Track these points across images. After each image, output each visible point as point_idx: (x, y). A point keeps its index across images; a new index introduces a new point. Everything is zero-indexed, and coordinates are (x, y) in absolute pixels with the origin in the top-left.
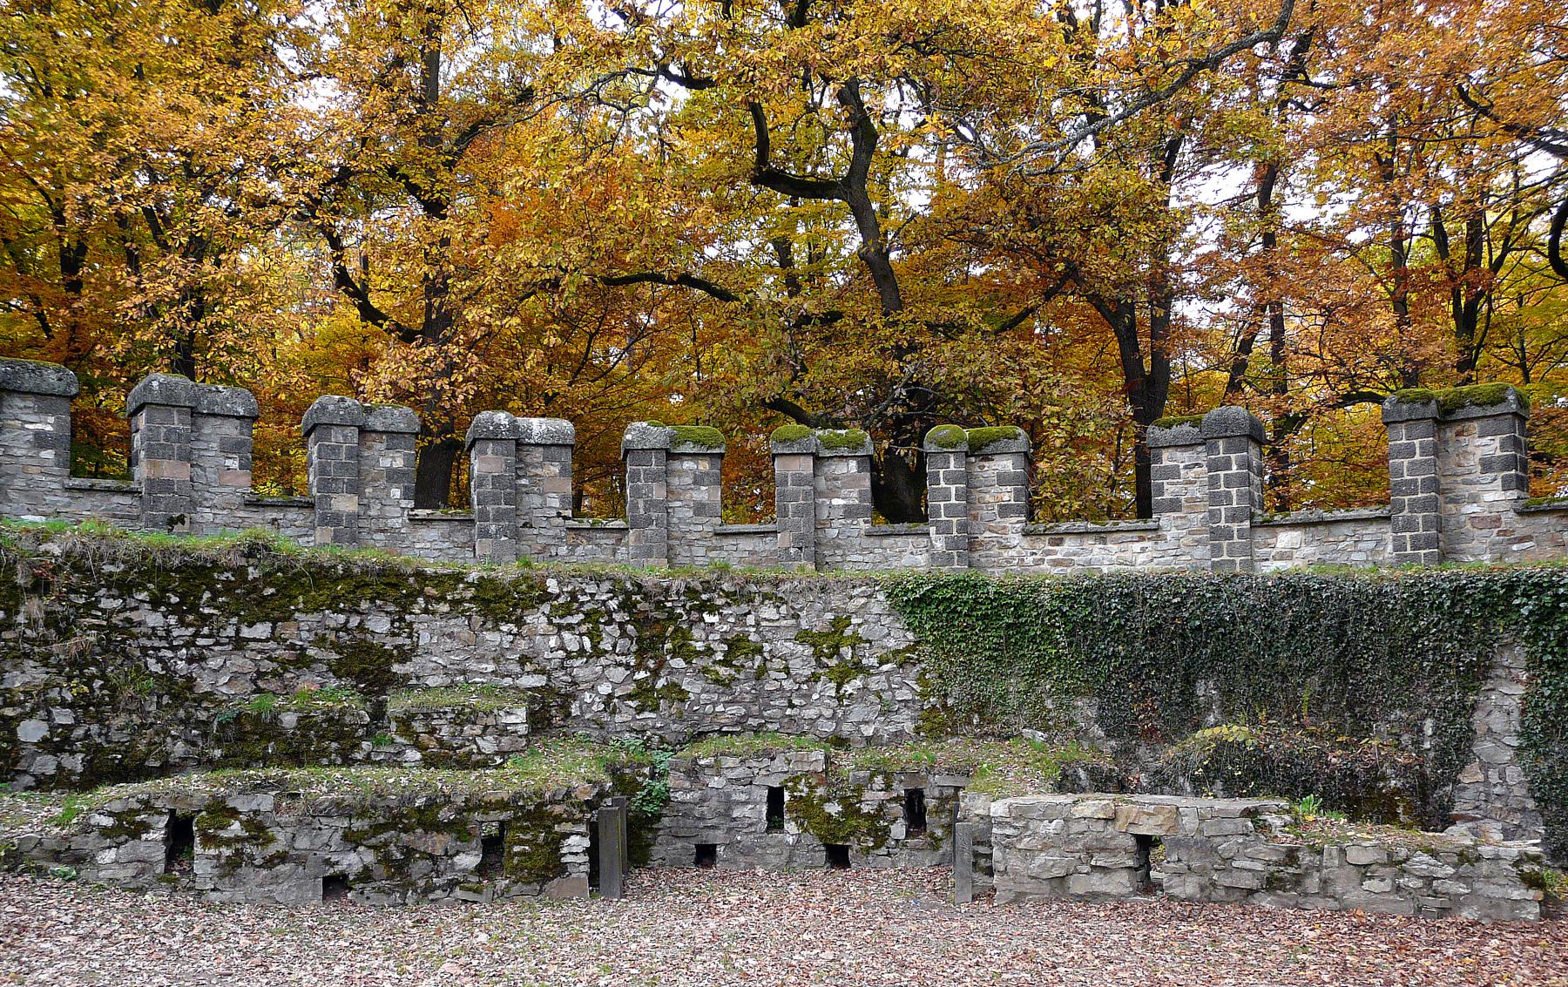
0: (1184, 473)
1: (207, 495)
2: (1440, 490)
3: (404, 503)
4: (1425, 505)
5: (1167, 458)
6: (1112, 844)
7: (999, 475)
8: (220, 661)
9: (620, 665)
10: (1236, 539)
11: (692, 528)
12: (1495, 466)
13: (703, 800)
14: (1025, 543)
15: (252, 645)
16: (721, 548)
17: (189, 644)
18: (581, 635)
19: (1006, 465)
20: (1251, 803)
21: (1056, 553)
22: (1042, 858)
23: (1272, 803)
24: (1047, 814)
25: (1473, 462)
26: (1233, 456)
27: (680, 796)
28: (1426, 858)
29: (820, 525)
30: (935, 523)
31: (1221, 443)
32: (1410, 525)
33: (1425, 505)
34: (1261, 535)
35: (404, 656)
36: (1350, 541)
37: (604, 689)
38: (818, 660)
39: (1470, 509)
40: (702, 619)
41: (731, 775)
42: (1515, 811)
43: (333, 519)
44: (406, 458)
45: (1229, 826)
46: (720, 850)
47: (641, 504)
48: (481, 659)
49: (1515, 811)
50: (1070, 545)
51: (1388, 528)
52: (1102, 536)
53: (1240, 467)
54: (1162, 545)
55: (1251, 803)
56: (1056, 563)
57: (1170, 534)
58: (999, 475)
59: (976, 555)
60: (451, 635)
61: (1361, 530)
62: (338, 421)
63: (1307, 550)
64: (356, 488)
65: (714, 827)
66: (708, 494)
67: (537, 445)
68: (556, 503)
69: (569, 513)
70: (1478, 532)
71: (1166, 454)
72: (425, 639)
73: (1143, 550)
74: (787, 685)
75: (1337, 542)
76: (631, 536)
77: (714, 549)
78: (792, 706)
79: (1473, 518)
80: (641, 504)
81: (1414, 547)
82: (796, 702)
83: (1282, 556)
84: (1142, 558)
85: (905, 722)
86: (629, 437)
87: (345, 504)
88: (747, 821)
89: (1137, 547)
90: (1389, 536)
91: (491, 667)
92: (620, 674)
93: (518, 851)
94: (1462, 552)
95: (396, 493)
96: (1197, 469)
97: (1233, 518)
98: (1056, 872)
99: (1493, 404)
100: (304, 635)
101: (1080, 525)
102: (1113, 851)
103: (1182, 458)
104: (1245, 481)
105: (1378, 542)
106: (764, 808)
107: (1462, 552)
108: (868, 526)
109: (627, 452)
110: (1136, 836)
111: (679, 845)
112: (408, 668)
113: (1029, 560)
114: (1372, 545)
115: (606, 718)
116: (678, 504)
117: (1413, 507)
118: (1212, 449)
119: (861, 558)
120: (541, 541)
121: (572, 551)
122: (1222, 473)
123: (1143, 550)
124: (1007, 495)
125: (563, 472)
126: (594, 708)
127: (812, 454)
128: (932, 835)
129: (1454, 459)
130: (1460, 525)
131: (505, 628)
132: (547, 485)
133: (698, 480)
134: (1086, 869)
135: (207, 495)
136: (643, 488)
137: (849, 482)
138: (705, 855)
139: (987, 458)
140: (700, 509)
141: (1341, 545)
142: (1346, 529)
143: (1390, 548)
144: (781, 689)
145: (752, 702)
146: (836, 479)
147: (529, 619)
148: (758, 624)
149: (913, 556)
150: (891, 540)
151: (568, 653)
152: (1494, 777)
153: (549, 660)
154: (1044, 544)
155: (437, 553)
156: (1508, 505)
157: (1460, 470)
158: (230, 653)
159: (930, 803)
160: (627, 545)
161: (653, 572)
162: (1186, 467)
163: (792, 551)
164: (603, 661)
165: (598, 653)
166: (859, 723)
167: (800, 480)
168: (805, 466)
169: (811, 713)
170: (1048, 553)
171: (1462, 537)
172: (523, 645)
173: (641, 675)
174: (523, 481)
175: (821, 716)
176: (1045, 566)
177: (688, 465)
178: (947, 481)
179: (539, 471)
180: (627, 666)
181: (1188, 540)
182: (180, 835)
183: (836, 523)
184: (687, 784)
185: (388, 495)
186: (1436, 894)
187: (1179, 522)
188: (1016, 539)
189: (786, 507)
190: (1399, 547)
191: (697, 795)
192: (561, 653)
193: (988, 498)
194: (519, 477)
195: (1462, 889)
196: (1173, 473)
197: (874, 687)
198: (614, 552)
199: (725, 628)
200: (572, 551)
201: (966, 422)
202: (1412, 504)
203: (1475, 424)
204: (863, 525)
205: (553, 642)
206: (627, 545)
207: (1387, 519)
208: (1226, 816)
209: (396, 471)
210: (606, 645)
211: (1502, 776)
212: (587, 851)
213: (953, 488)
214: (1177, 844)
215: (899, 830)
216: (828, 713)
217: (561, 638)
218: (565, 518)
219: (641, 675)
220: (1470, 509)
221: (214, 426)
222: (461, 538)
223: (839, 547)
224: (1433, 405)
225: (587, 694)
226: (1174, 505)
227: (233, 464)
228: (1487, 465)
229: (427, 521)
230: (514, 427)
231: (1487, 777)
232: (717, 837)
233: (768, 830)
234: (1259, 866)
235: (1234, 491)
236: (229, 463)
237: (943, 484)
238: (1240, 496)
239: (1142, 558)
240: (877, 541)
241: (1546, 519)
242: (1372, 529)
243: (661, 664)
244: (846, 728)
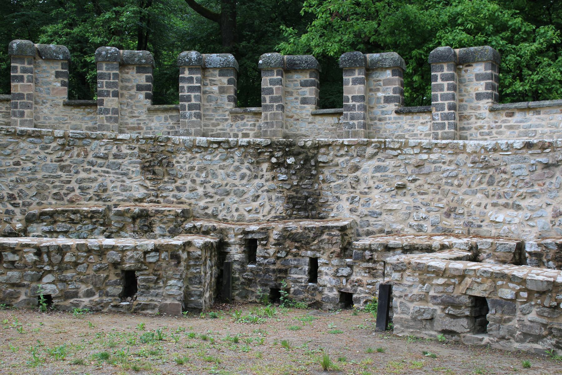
19: (479, 68)
60: (3, 364)
66: (310, 93)
110: (470, 296)
125: (229, 82)
137: (388, 84)
170: (504, 121)
178: (442, 80)
188: (485, 113)
229: (156, 110)
230: (199, 60)
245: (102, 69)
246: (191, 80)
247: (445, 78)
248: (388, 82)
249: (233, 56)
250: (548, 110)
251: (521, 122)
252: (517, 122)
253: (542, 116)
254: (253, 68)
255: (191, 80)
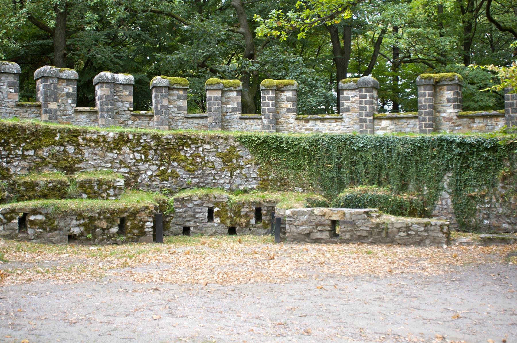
0: (351, 99)
1: (3, 102)
2: (435, 108)
3: (73, 105)
4: (429, 113)
5: (345, 94)
6: (324, 223)
7: (287, 98)
8: (17, 163)
9: (153, 164)
10: (368, 123)
11: (177, 115)
12: (451, 101)
13: (185, 212)
14: (296, 122)
15: (28, 158)
16: (187, 122)
17: (7, 157)
18: (141, 154)
20: (366, 210)
21: (306, 126)
22: (301, 228)
23: (373, 210)
24: (303, 213)
25: (444, 99)
26: (368, 94)
27: (178, 210)
28: (416, 225)
29: (224, 114)
30: (264, 115)
31: (364, 89)
32: (424, 120)
33: (429, 113)
34: (376, 122)
35: (81, 161)
36: (405, 124)
37: (149, 173)
38: (224, 163)
39: (444, 115)
40: (183, 149)
41: (196, 203)
42: (450, 213)
43: (48, 111)
44: (73, 88)
45: (360, 217)
46: (192, 229)
47: (159, 107)
48: (106, 162)
49: (450, 213)
50: (311, 123)
51: (417, 120)
52: (322, 120)
53: (370, 98)
54: (343, 124)
55: (366, 210)
56: (307, 129)
57: (346, 120)
58: (287, 98)
59: (278, 126)
60: (95, 154)
61: (409, 121)
62: (50, 75)
63: (392, 127)
64: (56, 100)
65: (189, 221)
67: (121, 84)
68: (128, 105)
69: (132, 109)
70: (446, 123)
71: (345, 92)
72: (86, 155)
73: (337, 125)
74: (214, 172)
75: (401, 125)
76: (155, 118)
77: (185, 123)
78: (215, 179)
79: (444, 118)
80: (159, 107)
81: (425, 127)
82: (217, 177)
83: (384, 129)
84: (336, 128)
85: (254, 184)
86: (155, 82)
87: (53, 106)
88: (201, 219)
89: (335, 124)
90: (418, 123)
91: (110, 165)
92: (154, 168)
93: (126, 228)
94: (441, 129)
95: (70, 101)
96: (356, 98)
97: (367, 115)
98: (307, 232)
99: (451, 81)
100: (45, 154)
101: (315, 116)
102: (324, 225)
103: (351, 94)
104: (372, 103)
105: (415, 125)
106: (207, 214)
107: (441, 129)
108: (240, 115)
109: (153, 87)
111: (177, 227)
112: (81, 165)
113: (297, 128)
114: (412, 126)
115: (150, 183)
116: (172, 106)
117: (426, 114)
118: (361, 91)
119: (237, 127)
120: (123, 119)
121: (133, 123)
122: (364, 100)
123: (337, 125)
124: (290, 105)
126: (146, 180)
127: (221, 89)
128: (264, 223)
129: (439, 98)
130: (440, 120)
131: (114, 152)
132: (124, 99)
133: (179, 98)
134: (316, 231)
135: (3, 102)
136: (157, 100)
137: (234, 100)
138: (186, 231)
139: (283, 91)
140: (179, 108)
141: (403, 126)
142: (404, 121)
143: (418, 127)
144: (211, 173)
145: (201, 178)
146: (229, 98)
147: (123, 148)
148: (203, 151)
149: (255, 128)
150: (248, 121)
151: (137, 160)
152: (444, 203)
153: (130, 163)
154: (302, 123)
155: (85, 124)
156: (454, 114)
157: (441, 102)
158: (20, 160)
159: (264, 212)
160: (153, 121)
161: (166, 133)
162: (352, 97)
163: (213, 124)
164: (149, 163)
165: (146, 161)
166: (238, 185)
167: (216, 99)
168: (218, 94)
169: (221, 181)
170: (304, 126)
171: (441, 124)
172: (121, 157)
173: (163, 168)
174: (116, 97)
175: (225, 182)
176: (303, 130)
177: (175, 92)
178: (269, 99)
179: (121, 94)
180: (157, 165)
181: (352, 122)
182: (23, 222)
183: (228, 114)
184: (180, 206)
185: (67, 102)
186: (419, 236)
187: (349, 116)
188: (292, 120)
189: (211, 108)
190: (420, 127)
191: (184, 210)
192: (134, 161)
193: (283, 106)
194: (114, 96)
195: (426, 234)
196: (347, 99)
197: (244, 172)
198: (149, 123)
199: (192, 152)
200: (133, 123)
201: (276, 78)
202: (425, 112)
203: (446, 87)
204: (238, 115)
205: (131, 156)
206: (153, 121)
207: (417, 117)
208: (359, 214)
209: (70, 93)
210: (150, 157)
211: (446, 202)
212: (152, 227)
213: (271, 102)
214: (345, 222)
215: (253, 221)
216: (227, 181)
217: (134, 155)
218: (131, 111)
219: (163, 168)
220: (444, 115)
221: (5, 77)
222: (93, 118)
223: (229, 122)
224: (432, 80)
225: (143, 175)
226: (348, 110)
227: (12, 91)
228: (449, 100)
231: (442, 203)
232: (191, 224)
233: (208, 221)
234: (368, 229)
235: (368, 106)
236: (11, 90)
237: (267, 101)
238: (370, 108)
239: (336, 128)
240: (243, 121)
241: (466, 119)
242: (412, 121)
243: (170, 164)
244: (234, 186)
245: (272, 103)
246: (424, 95)
247: (270, 99)
248: (235, 99)
249: (337, 227)
250: (328, 120)
251: (313, 126)
252: (311, 126)
253: (325, 124)
254: (75, 15)
255: (424, 95)
